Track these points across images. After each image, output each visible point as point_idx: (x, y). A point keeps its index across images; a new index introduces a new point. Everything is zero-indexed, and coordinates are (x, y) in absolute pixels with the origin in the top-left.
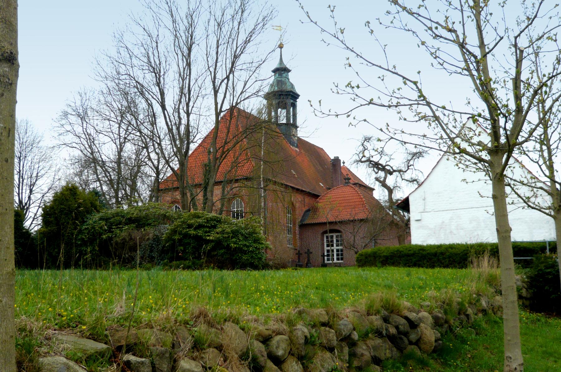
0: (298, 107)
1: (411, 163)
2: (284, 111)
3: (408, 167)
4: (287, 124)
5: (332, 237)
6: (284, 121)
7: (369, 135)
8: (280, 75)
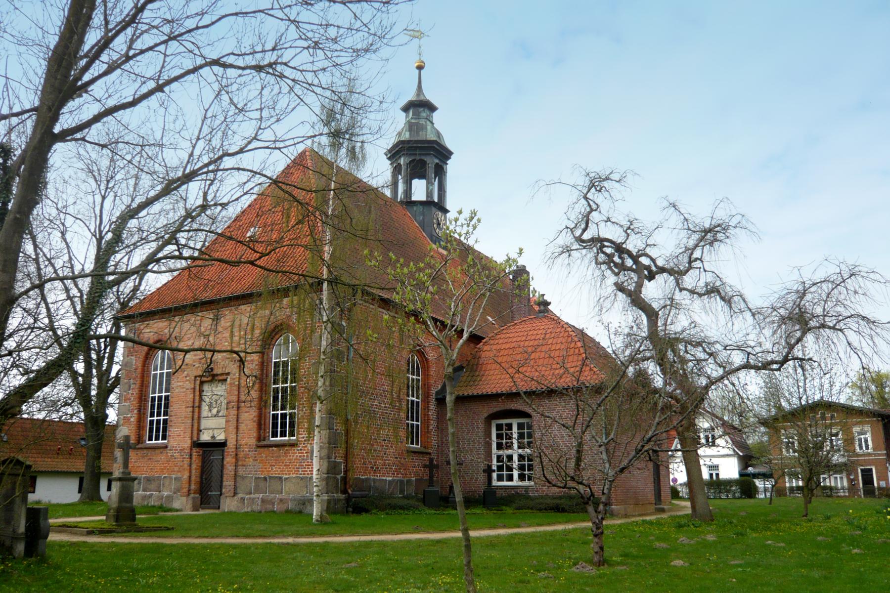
0: (448, 175)
1: (697, 254)
2: (423, 182)
3: (690, 262)
4: (428, 204)
5: (510, 427)
6: (423, 198)
7: (598, 168)
8: (417, 115)
